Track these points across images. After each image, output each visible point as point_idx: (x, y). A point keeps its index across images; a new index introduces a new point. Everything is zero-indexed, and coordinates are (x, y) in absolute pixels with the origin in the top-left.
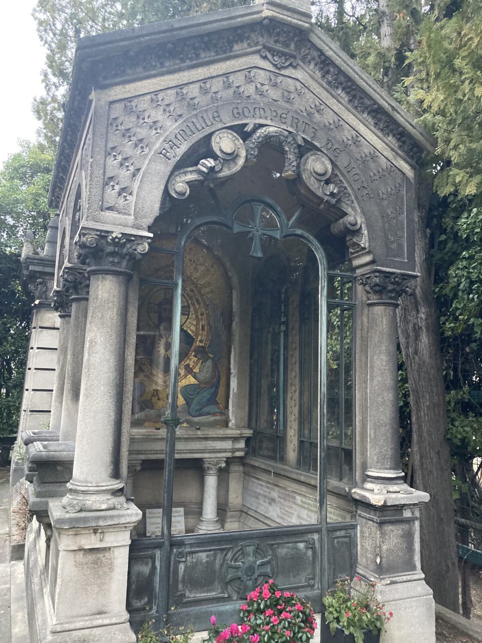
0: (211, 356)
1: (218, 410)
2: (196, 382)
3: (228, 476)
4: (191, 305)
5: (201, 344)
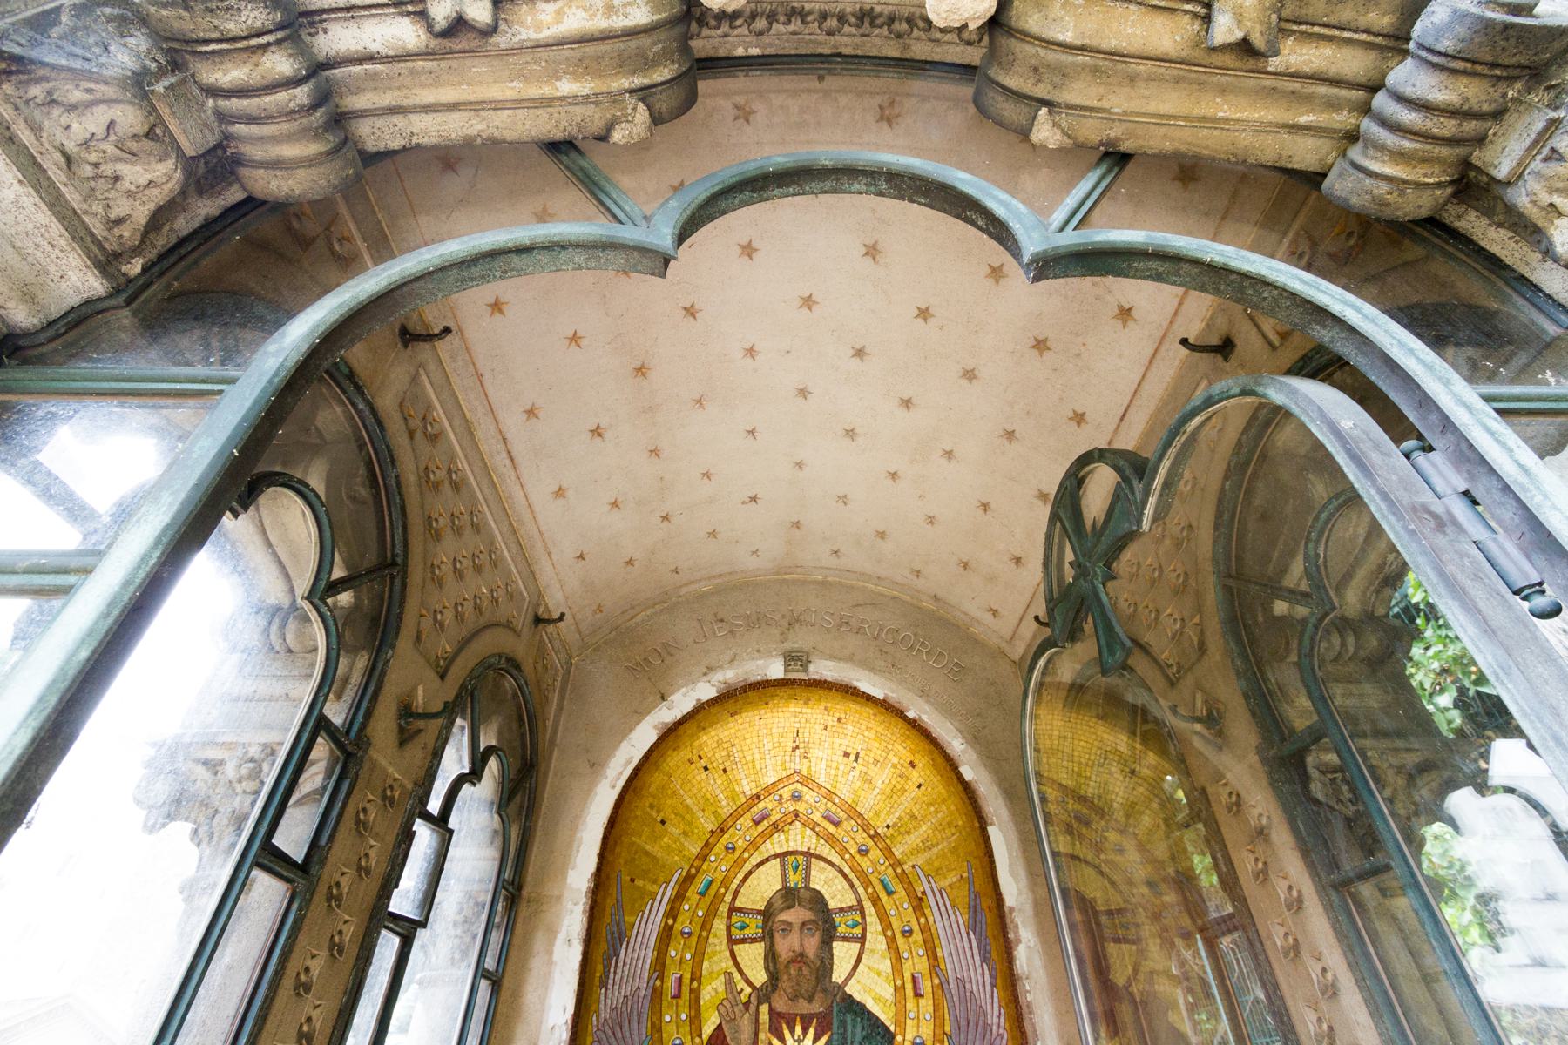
4: (867, 905)
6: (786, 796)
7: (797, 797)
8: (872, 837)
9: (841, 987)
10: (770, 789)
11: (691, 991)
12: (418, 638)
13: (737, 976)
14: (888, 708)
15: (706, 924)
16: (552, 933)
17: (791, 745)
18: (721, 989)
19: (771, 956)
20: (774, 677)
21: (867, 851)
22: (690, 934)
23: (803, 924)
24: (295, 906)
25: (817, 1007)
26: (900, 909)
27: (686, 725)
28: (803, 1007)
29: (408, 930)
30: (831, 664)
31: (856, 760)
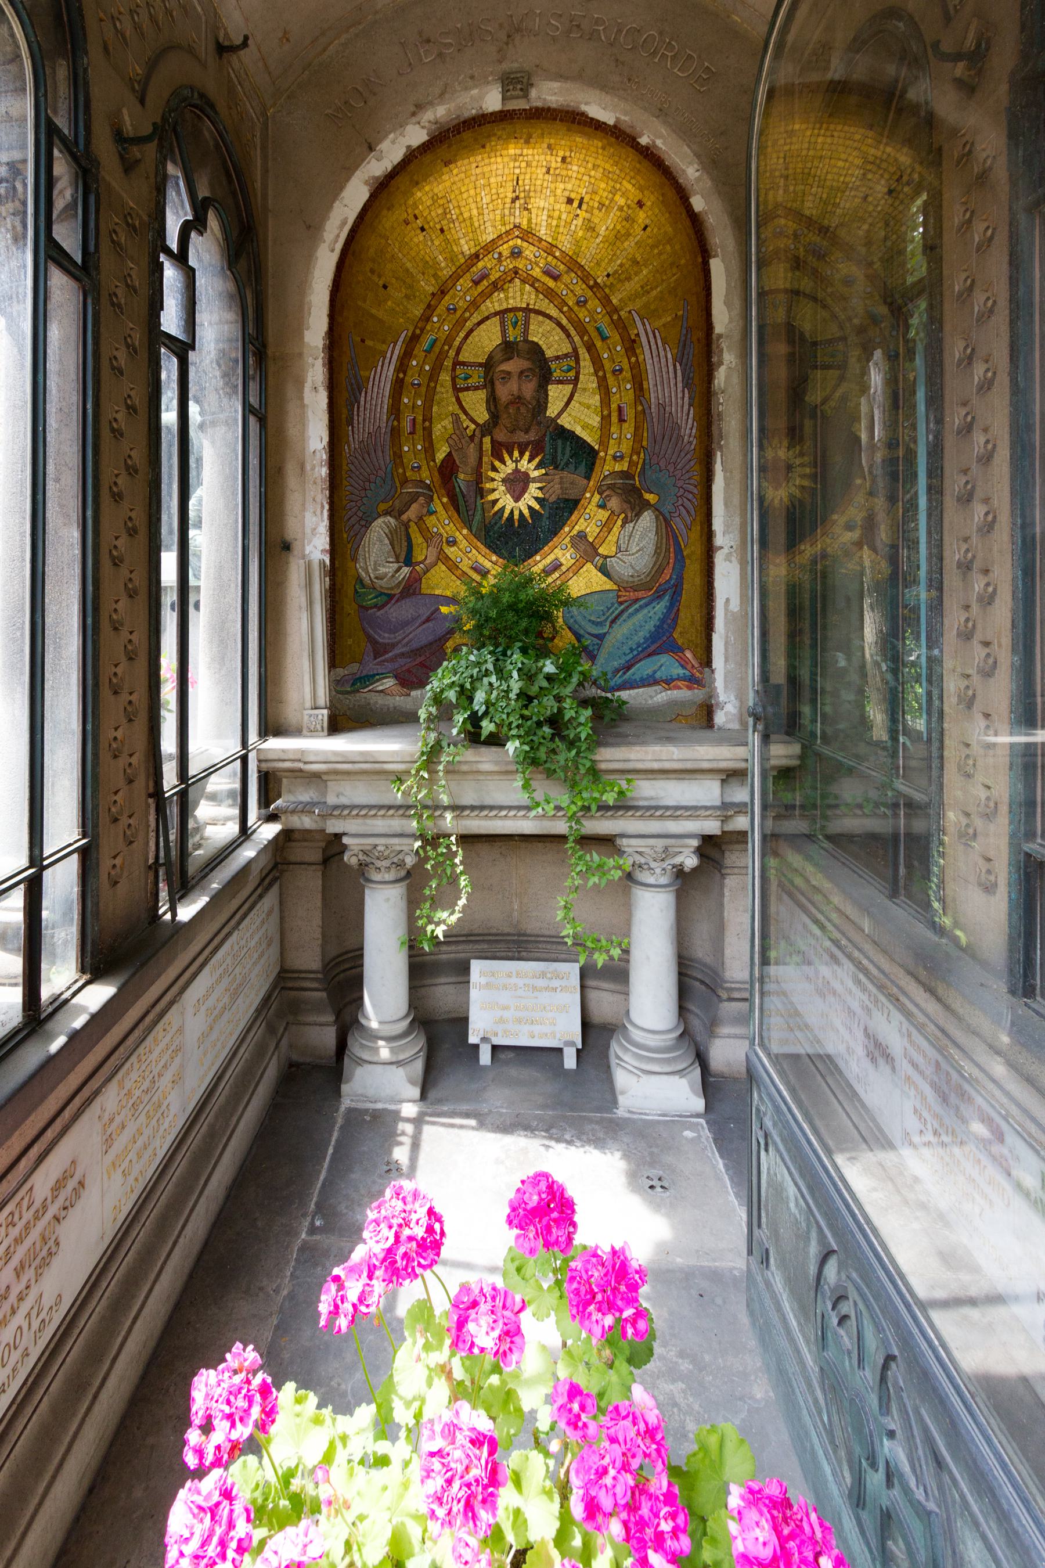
0: (651, 497)
1: (681, 671)
2: (609, 585)
3: (722, 887)
4: (583, 353)
5: (618, 467)
6: (506, 253)
7: (516, 253)
8: (591, 288)
9: (553, 420)
10: (489, 248)
11: (424, 429)
12: (106, 49)
13: (463, 417)
14: (619, 136)
15: (433, 376)
16: (300, 383)
17: (511, 195)
18: (450, 426)
19: (492, 400)
20: (490, 110)
21: (586, 302)
22: (419, 385)
23: (522, 372)
24: (89, 301)
25: (532, 436)
26: (612, 352)
27: (398, 179)
28: (521, 437)
29: (183, 349)
30: (556, 85)
31: (580, 206)
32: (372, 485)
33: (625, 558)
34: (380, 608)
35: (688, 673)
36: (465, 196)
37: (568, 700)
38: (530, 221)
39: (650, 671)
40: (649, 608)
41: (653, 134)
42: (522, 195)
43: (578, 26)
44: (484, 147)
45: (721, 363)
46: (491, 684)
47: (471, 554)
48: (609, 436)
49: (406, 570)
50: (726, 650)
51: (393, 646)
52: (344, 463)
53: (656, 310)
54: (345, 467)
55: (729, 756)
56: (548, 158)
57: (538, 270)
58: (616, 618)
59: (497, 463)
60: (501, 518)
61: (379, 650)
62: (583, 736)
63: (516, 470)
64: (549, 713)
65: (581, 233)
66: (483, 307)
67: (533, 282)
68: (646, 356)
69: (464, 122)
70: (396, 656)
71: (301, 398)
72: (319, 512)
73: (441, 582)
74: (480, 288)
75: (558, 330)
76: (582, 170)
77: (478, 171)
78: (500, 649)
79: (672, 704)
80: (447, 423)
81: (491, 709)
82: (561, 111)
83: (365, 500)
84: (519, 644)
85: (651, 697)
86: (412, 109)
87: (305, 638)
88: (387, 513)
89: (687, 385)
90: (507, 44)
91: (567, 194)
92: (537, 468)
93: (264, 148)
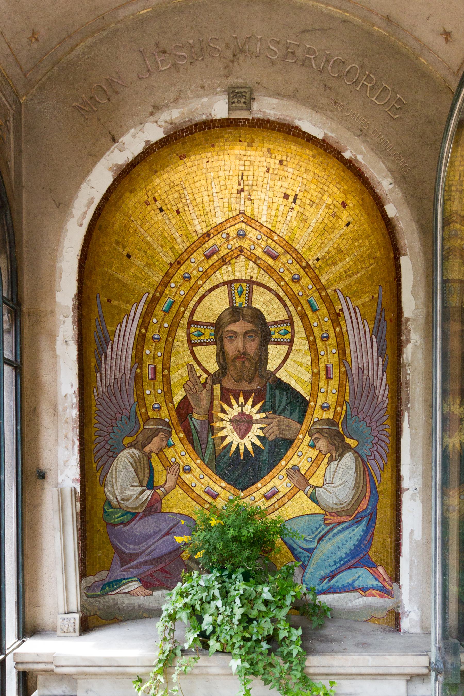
0: (352, 443)
1: (375, 583)
4: (296, 319)
5: (325, 415)
7: (241, 235)
8: (304, 268)
10: (219, 229)
11: (163, 376)
13: (197, 367)
14: (327, 149)
15: (171, 332)
16: (52, 337)
18: (185, 375)
19: (221, 355)
20: (218, 117)
21: (299, 279)
22: (159, 339)
23: (246, 333)
25: (255, 386)
26: (321, 321)
27: (139, 168)
28: (245, 386)
30: (274, 101)
31: (294, 201)
32: (119, 423)
33: (329, 489)
34: (126, 524)
35: (380, 585)
36: (198, 184)
37: (282, 623)
38: (252, 209)
39: (350, 581)
40: (350, 530)
41: (355, 150)
42: (246, 188)
43: (293, 53)
44: (213, 146)
45: (408, 341)
46: (217, 608)
47: (202, 478)
48: (318, 390)
49: (148, 493)
50: (411, 570)
51: (138, 555)
52: (94, 403)
53: (357, 291)
54: (93, 408)
55: (413, 663)
56: (268, 160)
57: (260, 250)
58: (323, 536)
59: (226, 407)
60: (228, 451)
61: (125, 559)
62: (295, 653)
63: (242, 413)
64: (266, 634)
65: (295, 223)
66: (213, 277)
67: (256, 260)
68: (347, 326)
69: (196, 125)
70: (140, 564)
71: (54, 350)
72: (70, 447)
73: (178, 503)
74: (211, 262)
75: (277, 300)
76: (296, 172)
77: (209, 165)
78: (226, 573)
79: (369, 607)
80: (184, 372)
81: (218, 629)
82: (278, 123)
83: (112, 435)
84: (242, 570)
85: (351, 601)
86: (151, 109)
87: (59, 554)
88: (131, 445)
89: (381, 355)
90: (233, 62)
91: (283, 190)
92: (259, 412)
93: (17, 130)
